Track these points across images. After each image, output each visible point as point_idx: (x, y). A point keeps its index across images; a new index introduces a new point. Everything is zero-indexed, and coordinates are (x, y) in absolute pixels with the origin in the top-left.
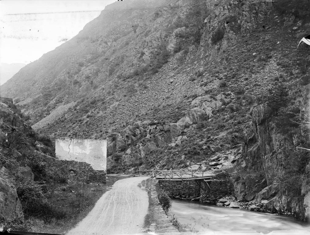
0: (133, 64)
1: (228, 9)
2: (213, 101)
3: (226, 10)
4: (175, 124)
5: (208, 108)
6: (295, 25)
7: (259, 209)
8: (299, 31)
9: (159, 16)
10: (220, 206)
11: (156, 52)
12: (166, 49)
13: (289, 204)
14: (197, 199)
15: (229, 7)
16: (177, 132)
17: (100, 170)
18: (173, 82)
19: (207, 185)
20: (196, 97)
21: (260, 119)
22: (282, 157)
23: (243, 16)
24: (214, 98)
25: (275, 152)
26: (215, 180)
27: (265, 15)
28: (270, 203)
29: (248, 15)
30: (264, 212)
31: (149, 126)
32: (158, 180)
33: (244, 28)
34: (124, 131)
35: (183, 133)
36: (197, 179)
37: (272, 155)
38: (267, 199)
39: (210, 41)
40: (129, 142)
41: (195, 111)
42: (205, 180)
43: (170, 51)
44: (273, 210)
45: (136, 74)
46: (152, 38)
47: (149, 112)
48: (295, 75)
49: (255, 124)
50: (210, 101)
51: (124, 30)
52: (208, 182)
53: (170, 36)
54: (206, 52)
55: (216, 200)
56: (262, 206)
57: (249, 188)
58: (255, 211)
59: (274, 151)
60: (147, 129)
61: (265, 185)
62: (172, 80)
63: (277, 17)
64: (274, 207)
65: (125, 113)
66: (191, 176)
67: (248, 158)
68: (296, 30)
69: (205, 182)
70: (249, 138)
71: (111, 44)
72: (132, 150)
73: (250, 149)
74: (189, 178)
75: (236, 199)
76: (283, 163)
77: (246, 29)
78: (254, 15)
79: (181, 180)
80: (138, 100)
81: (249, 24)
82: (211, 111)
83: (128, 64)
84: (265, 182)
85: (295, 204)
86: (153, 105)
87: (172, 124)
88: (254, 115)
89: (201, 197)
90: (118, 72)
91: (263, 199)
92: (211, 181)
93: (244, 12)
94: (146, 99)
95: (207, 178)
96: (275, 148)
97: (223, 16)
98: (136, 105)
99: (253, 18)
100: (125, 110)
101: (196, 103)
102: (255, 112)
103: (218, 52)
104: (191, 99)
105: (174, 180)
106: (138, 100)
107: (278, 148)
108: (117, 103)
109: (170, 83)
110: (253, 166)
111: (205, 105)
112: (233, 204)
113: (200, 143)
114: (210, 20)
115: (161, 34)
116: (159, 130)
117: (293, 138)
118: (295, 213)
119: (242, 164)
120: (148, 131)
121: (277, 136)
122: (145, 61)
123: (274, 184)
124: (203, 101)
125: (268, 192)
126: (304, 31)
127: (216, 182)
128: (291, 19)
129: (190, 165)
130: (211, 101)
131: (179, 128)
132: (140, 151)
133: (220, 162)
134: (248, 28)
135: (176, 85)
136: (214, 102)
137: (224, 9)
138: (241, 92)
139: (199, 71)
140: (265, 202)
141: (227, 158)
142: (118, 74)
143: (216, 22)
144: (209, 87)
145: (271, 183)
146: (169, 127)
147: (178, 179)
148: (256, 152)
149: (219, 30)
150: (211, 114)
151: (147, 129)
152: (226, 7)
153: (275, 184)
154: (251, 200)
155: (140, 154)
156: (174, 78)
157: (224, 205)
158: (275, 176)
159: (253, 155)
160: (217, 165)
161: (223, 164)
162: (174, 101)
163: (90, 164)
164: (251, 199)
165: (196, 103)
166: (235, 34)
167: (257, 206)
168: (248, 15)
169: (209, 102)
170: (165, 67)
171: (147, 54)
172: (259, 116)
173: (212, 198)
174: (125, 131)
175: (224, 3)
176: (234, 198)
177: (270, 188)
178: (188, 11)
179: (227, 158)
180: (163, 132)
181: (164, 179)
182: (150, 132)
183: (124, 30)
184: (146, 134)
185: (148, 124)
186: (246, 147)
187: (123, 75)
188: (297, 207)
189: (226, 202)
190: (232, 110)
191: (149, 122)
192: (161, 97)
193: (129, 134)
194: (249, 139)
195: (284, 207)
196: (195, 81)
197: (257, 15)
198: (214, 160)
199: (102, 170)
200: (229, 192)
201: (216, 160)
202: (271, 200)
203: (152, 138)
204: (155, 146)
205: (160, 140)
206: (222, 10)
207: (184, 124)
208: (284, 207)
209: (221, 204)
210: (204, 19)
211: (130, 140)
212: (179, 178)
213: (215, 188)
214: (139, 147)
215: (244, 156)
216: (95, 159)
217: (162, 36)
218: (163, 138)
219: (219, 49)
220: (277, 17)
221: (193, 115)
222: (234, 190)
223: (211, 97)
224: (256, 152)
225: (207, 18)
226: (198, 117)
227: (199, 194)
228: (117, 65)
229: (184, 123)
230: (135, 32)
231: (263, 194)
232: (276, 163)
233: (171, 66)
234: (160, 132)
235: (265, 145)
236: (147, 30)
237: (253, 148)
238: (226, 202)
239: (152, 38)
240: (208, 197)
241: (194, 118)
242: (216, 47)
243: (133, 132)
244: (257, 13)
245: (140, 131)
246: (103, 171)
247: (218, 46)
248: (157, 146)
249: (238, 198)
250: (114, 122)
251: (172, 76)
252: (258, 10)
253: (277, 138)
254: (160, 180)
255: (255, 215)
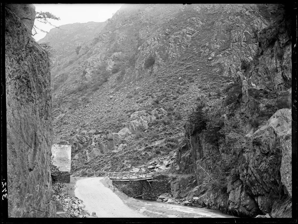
0: (76, 81)
1: (158, 40)
2: (148, 115)
3: (156, 41)
4: (117, 133)
5: (144, 121)
6: (209, 56)
7: (191, 204)
8: (213, 61)
9: (99, 40)
10: (159, 202)
11: (97, 71)
12: (105, 70)
13: (215, 199)
14: (139, 197)
15: (158, 38)
16: (118, 141)
17: (66, 171)
18: (112, 98)
19: (149, 184)
20: (135, 111)
21: (192, 131)
22: (210, 162)
23: (169, 46)
24: (150, 114)
25: (205, 158)
26: (155, 180)
27: (187, 47)
28: (200, 199)
29: (173, 46)
30: (195, 206)
31: (94, 135)
32: (112, 180)
33: (170, 56)
34: (72, 139)
35: (123, 142)
36: (142, 179)
37: (202, 160)
38: (198, 196)
39: (143, 66)
40: (77, 149)
41: (134, 123)
42: (147, 181)
43: (108, 71)
44: (203, 205)
45: (80, 90)
46: (93, 59)
47: (92, 123)
48: (213, 97)
49: (188, 134)
50: (145, 115)
51: (67, 51)
52: (150, 182)
53: (109, 59)
54: (140, 75)
55: (156, 197)
56: (194, 202)
57: (183, 187)
58: (188, 206)
59: (204, 157)
60: (93, 137)
61: (196, 184)
62: (111, 97)
63: (195, 49)
64: (204, 202)
65: (71, 123)
66: (136, 177)
67: (182, 163)
68: (211, 60)
69: (148, 182)
70: (182, 147)
71: (55, 63)
72: (79, 156)
73: (183, 155)
74: (135, 179)
75: (172, 196)
76: (211, 167)
77: (172, 57)
78: (178, 47)
79: (129, 180)
80: (81, 113)
81: (175, 54)
82: (147, 124)
83: (72, 81)
84: (196, 182)
85: (221, 200)
86: (95, 117)
87: (114, 134)
88: (187, 128)
89: (143, 194)
90: (63, 87)
91: (194, 196)
92: (152, 181)
93: (170, 44)
94: (89, 112)
95: (150, 178)
96: (205, 154)
97: (154, 45)
98: (80, 117)
99: (177, 49)
100: (70, 121)
101: (134, 117)
102: (188, 125)
103: (150, 75)
104: (129, 113)
105: (123, 180)
106: (81, 113)
107: (207, 154)
108: (64, 115)
109: (110, 99)
110: (185, 169)
111: (142, 119)
112: (170, 200)
113: (140, 150)
114: (143, 48)
115: (101, 56)
116: (104, 138)
117: (219, 147)
118: (220, 207)
119: (176, 168)
120: (94, 139)
121: (206, 145)
122: (88, 78)
123: (204, 184)
124: (140, 115)
125: (199, 190)
126: (217, 61)
127: (157, 181)
128: (206, 51)
129: (131, 168)
130: (147, 115)
131: (120, 137)
132: (86, 157)
133: (157, 166)
134: (174, 56)
135: (116, 100)
136: (149, 116)
137: (154, 40)
138: (171, 109)
139: (135, 90)
140: (196, 198)
141: (162, 163)
142: (62, 89)
143: (148, 50)
144: (146, 103)
145: (201, 184)
146: (111, 136)
147: (126, 179)
148: (188, 158)
149: (151, 57)
150: (147, 127)
151: (93, 137)
152: (156, 39)
153: (204, 184)
154: (185, 197)
155: (86, 159)
156: (113, 95)
157: (162, 201)
158: (205, 178)
159: (186, 160)
160: (153, 168)
161: (159, 167)
162: (115, 114)
163: (56, 166)
164: (185, 196)
165: (134, 117)
166: (164, 61)
167: (190, 202)
168: (173, 46)
169: (145, 116)
170: (105, 85)
171: (89, 73)
172: (191, 128)
173: (152, 196)
174: (73, 139)
175: (154, 36)
176: (170, 196)
177: (200, 187)
178: (124, 39)
179: (162, 163)
180: (107, 140)
181: (115, 179)
182: (95, 140)
183: (67, 51)
184: (92, 142)
185: (93, 133)
186: (179, 154)
187: (67, 90)
188: (223, 202)
189: (164, 198)
190: (165, 124)
191: (94, 131)
192: (102, 110)
193: (76, 141)
194: (183, 147)
195: (212, 202)
196: (133, 98)
197: (180, 46)
198: (151, 165)
199: (67, 171)
200: (167, 189)
201: (153, 164)
202: (201, 197)
203: (97, 145)
204: (100, 152)
205: (104, 147)
206: (153, 40)
207: (124, 134)
208: (212, 202)
209: (160, 200)
210: (138, 47)
211: (77, 147)
212: (127, 179)
213: (155, 187)
214: (85, 153)
215: (178, 162)
216: (61, 161)
217: (102, 58)
218: (106, 146)
219: (151, 73)
220: (195, 49)
221: (132, 127)
222: (170, 189)
223: (147, 112)
224: (188, 158)
225: (141, 46)
226: (137, 129)
227: (142, 193)
228: (61, 81)
229: (125, 133)
230: (78, 53)
231: (195, 192)
232: (205, 167)
233: (110, 84)
234: (104, 140)
235: (196, 152)
236: (89, 52)
237: (186, 154)
238: (164, 198)
239: (93, 59)
240: (149, 195)
241: (133, 129)
242: (149, 71)
243: (80, 139)
244: (180, 45)
245: (87, 139)
246: (68, 172)
247: (150, 70)
248: (102, 152)
249: (174, 195)
250: (61, 131)
251: (111, 93)
252: (181, 43)
253: (206, 147)
254: (113, 180)
255: (191, 209)
